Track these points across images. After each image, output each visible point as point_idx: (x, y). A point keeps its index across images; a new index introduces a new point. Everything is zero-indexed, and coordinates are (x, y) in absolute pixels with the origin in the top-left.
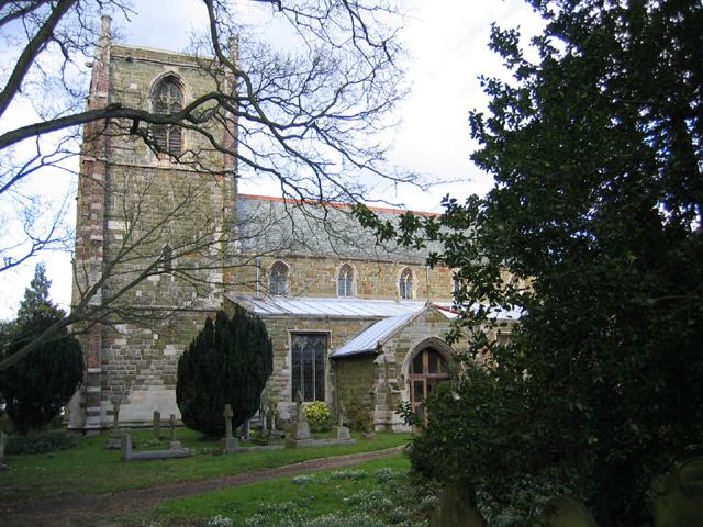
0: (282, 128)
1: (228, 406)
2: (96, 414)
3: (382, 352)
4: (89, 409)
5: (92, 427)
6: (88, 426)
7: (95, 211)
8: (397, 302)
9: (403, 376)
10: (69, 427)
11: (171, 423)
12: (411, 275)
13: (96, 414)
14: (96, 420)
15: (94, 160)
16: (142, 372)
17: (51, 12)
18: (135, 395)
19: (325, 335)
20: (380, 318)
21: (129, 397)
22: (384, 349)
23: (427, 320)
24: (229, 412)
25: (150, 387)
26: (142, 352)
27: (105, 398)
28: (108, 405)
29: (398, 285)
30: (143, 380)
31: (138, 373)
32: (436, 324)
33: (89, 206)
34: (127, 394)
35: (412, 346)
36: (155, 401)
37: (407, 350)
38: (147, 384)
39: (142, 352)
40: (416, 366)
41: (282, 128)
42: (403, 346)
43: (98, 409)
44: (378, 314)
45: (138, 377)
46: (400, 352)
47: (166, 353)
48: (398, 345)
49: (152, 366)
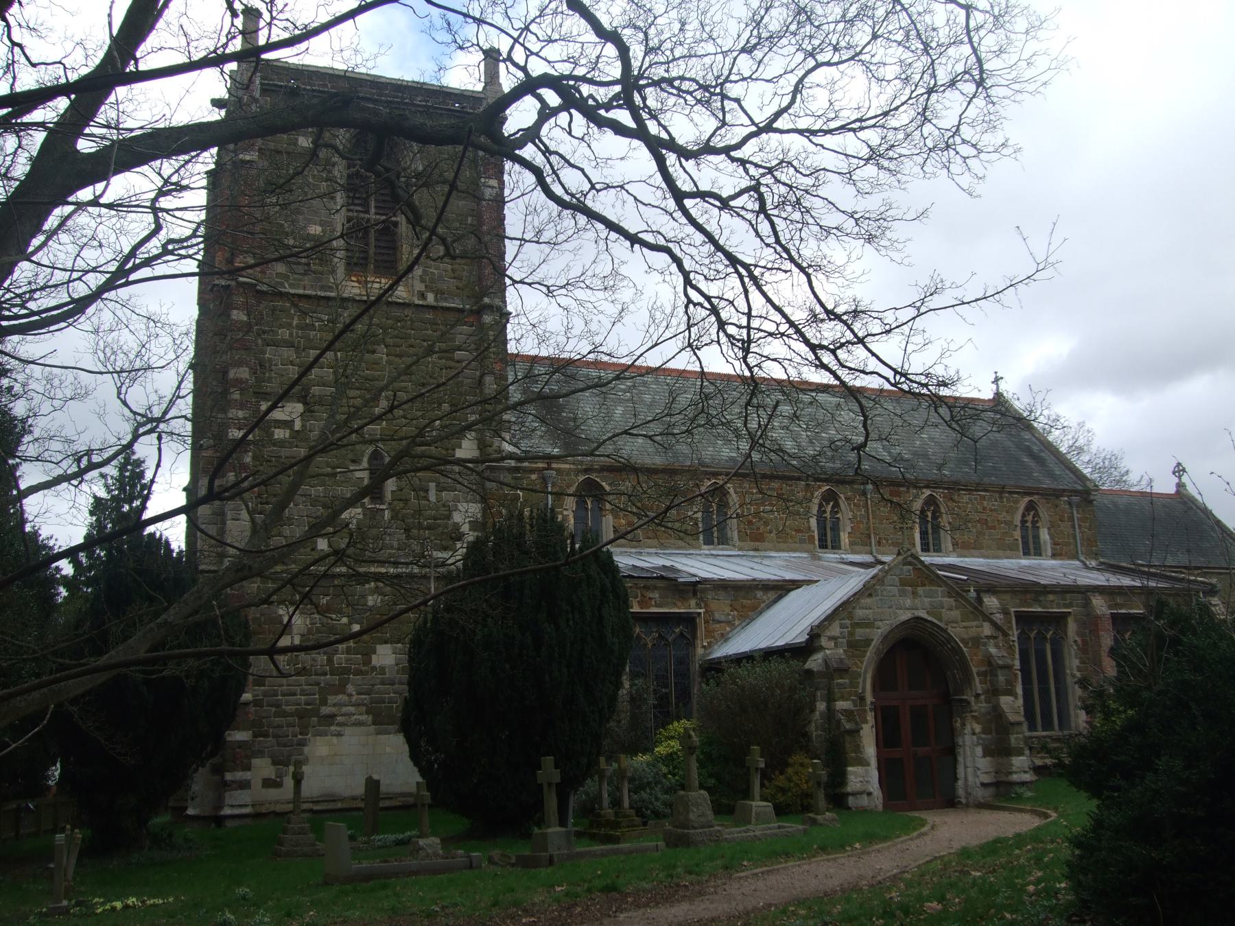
0: (684, 153)
1: (548, 761)
2: (244, 785)
3: (821, 648)
4: (229, 776)
5: (236, 811)
6: (227, 811)
7: (238, 382)
8: (815, 557)
9: (862, 699)
10: (190, 812)
11: (406, 808)
12: (837, 505)
13: (244, 785)
14: (243, 796)
15: (233, 283)
16: (332, 699)
17: (108, 42)
18: (319, 747)
19: (689, 621)
20: (795, 585)
21: (306, 750)
22: (824, 642)
23: (903, 583)
24: (549, 771)
25: (348, 730)
26: (330, 661)
27: (260, 754)
28: (263, 768)
29: (813, 522)
30: (332, 716)
31: (324, 702)
32: (920, 590)
33: (225, 373)
34: (302, 744)
35: (876, 635)
36: (358, 756)
37: (868, 642)
38: (339, 724)
39: (330, 661)
40: (884, 677)
41: (684, 153)
42: (860, 633)
43: (247, 775)
44: (789, 576)
45: (325, 710)
46: (856, 647)
47: (375, 661)
48: (851, 634)
49: (350, 688)
